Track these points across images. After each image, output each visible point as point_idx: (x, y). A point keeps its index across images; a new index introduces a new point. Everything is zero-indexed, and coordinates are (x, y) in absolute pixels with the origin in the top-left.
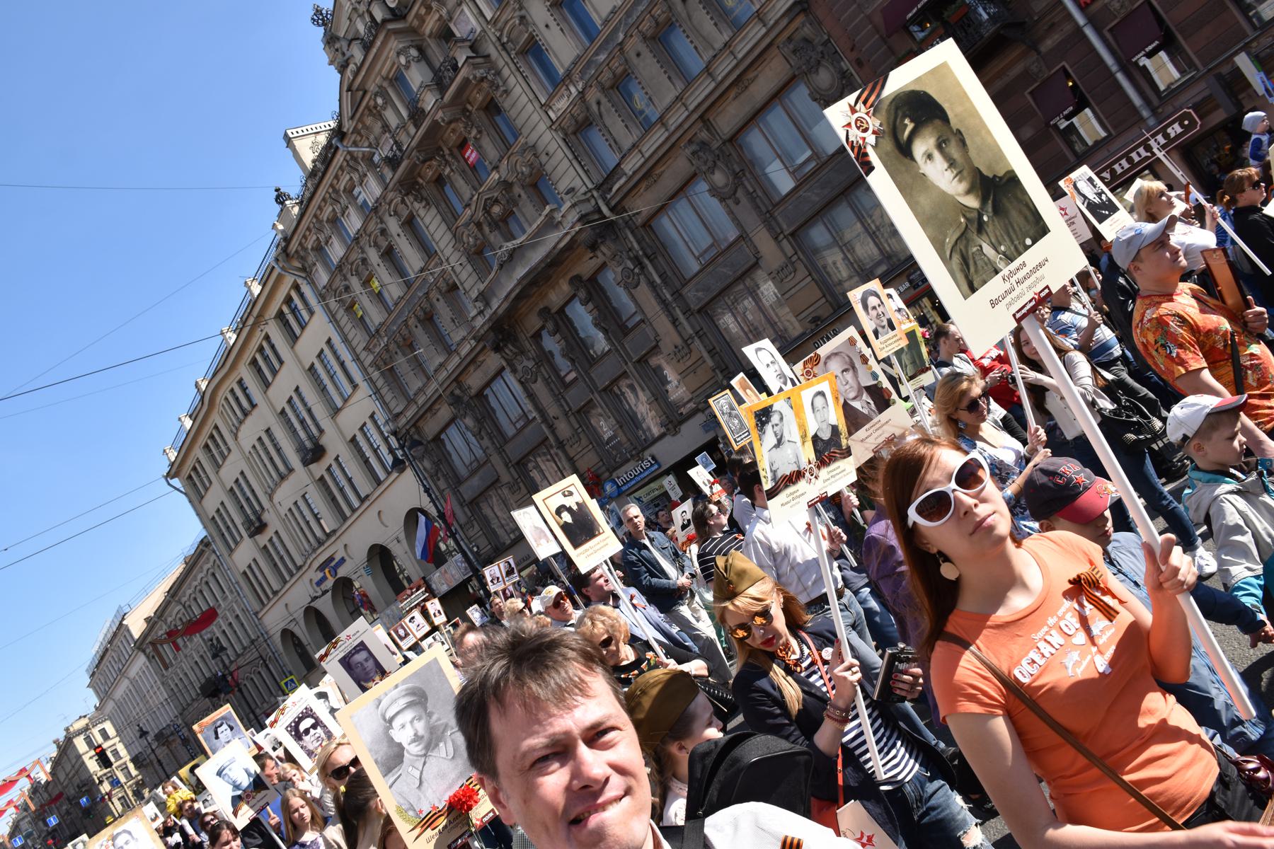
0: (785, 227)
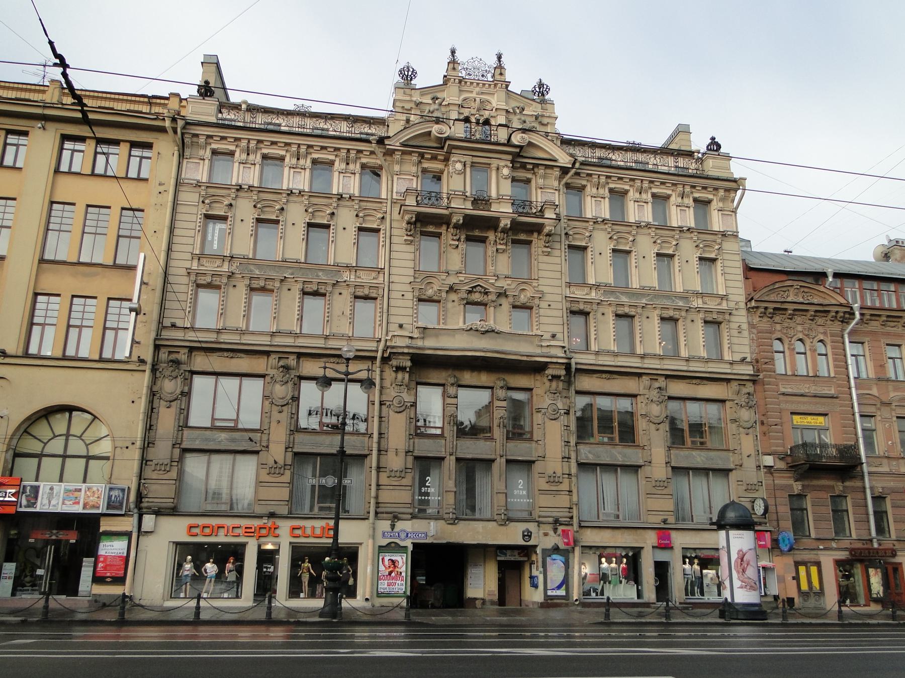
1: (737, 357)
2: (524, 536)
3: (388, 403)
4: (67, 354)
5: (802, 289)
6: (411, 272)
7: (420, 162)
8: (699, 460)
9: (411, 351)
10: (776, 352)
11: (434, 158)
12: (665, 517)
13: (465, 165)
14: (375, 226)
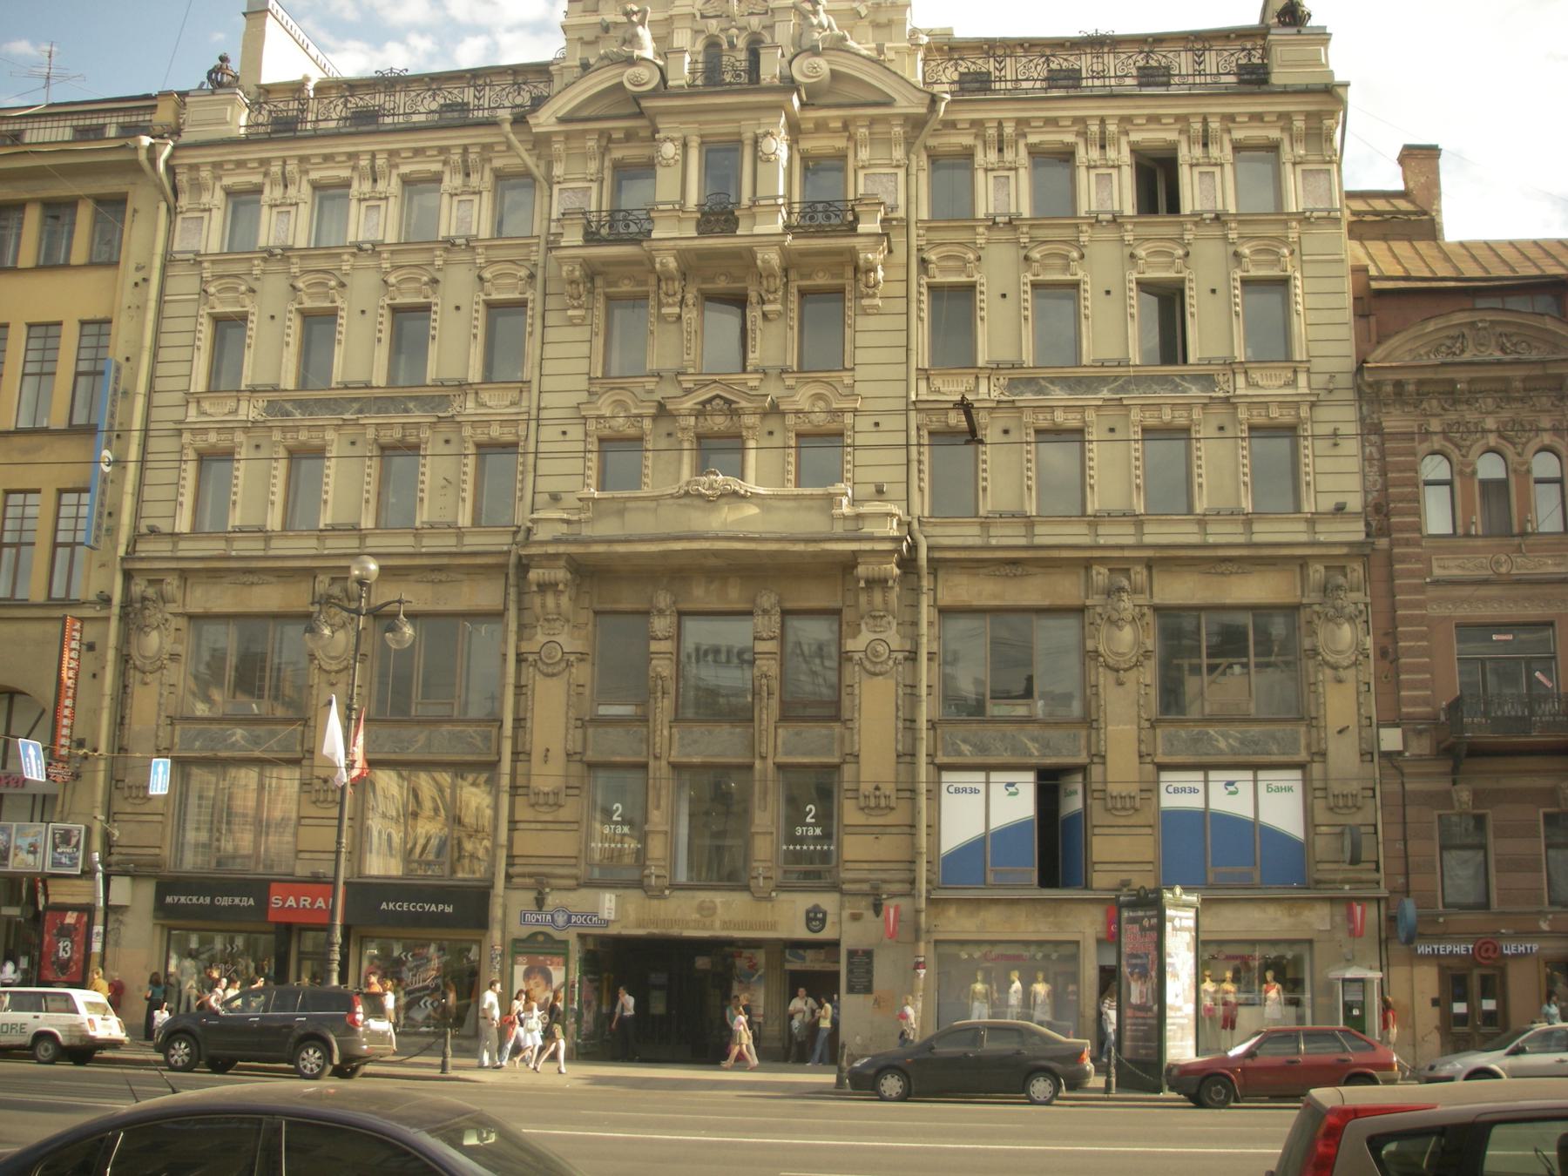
0: (1160, 751)
1: (1327, 503)
2: (809, 920)
3: (531, 658)
4: (54, 595)
5: (1499, 329)
6: (582, 383)
7: (604, 151)
8: (1222, 744)
9: (573, 549)
10: (1428, 483)
11: (630, 136)
12: (1124, 876)
13: (685, 145)
14: (516, 295)
